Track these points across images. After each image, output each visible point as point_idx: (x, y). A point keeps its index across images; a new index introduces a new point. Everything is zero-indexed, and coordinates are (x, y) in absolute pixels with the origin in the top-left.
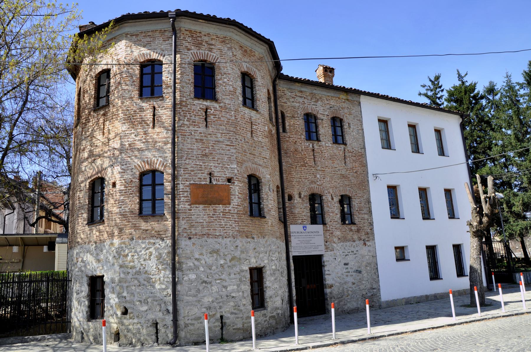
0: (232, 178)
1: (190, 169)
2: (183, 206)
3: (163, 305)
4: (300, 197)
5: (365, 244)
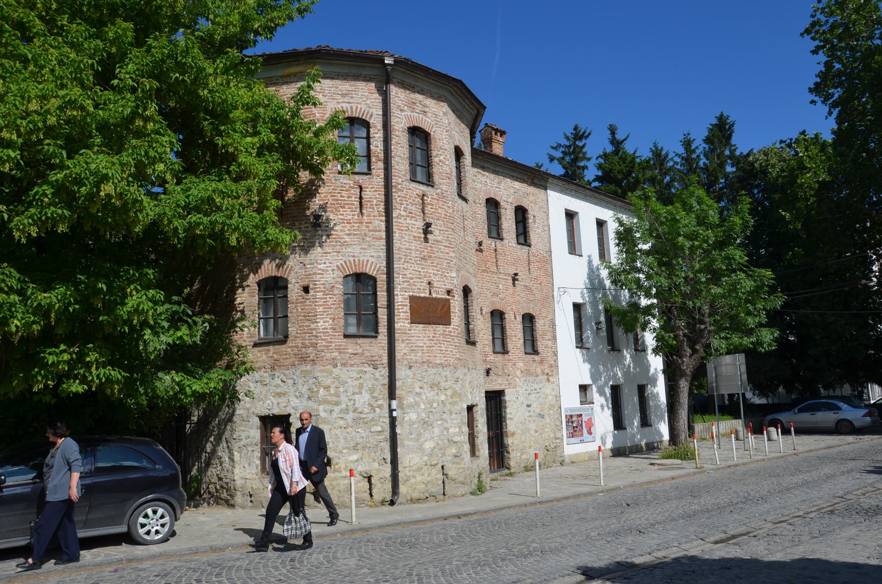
1: (409, 276)
5: (548, 380)
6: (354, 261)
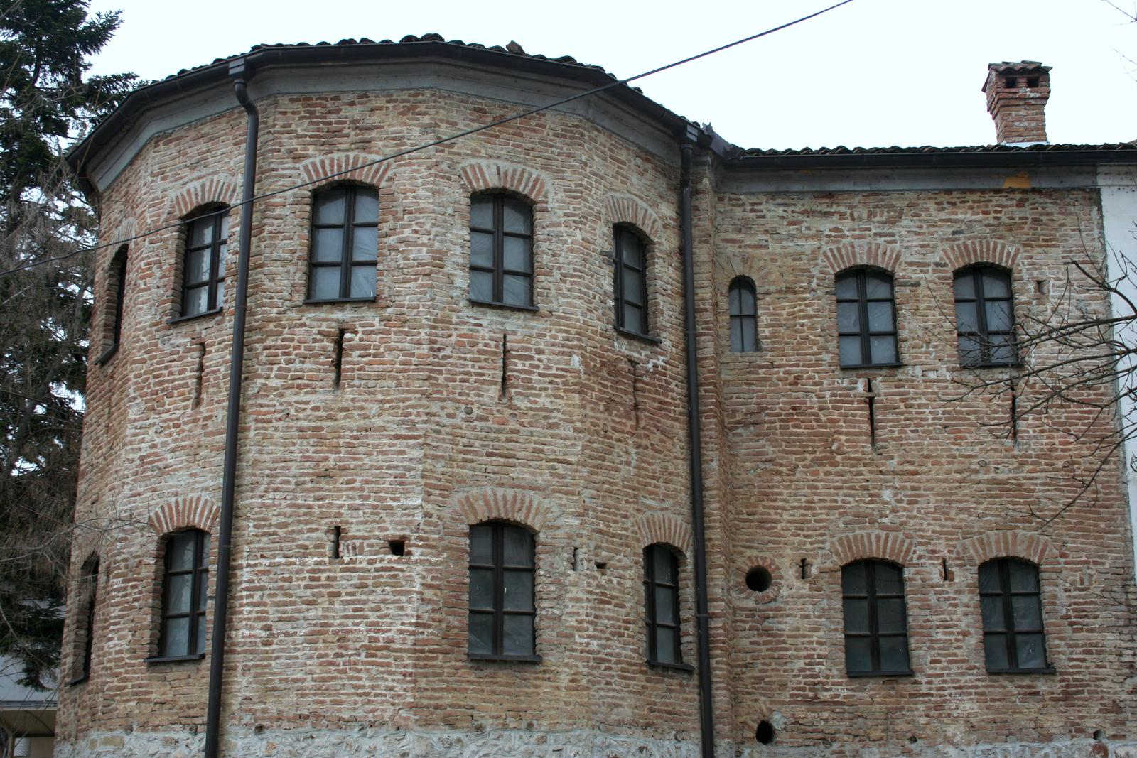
0: (405, 538)
1: (274, 521)
2: (246, 632)
4: (803, 575)
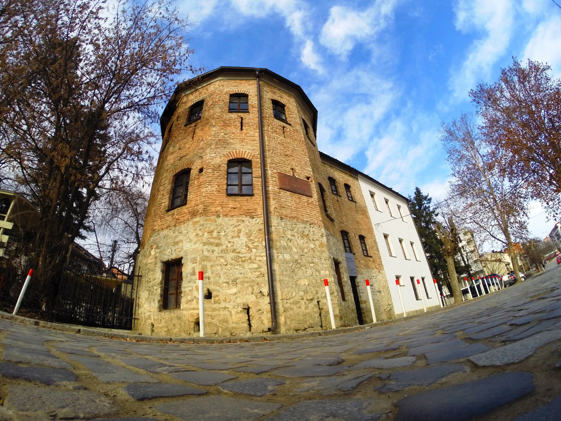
3: (255, 287)
6: (236, 152)
